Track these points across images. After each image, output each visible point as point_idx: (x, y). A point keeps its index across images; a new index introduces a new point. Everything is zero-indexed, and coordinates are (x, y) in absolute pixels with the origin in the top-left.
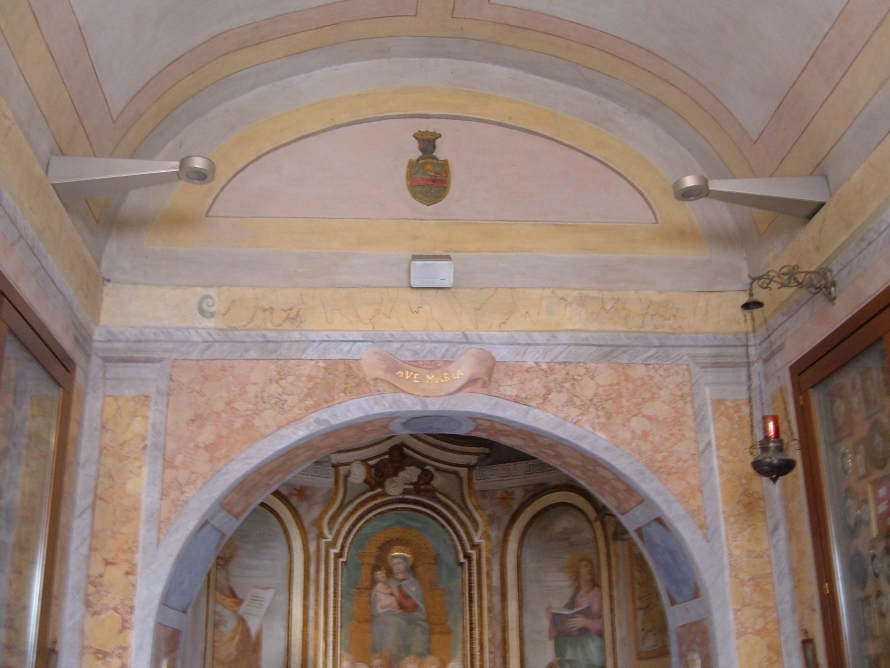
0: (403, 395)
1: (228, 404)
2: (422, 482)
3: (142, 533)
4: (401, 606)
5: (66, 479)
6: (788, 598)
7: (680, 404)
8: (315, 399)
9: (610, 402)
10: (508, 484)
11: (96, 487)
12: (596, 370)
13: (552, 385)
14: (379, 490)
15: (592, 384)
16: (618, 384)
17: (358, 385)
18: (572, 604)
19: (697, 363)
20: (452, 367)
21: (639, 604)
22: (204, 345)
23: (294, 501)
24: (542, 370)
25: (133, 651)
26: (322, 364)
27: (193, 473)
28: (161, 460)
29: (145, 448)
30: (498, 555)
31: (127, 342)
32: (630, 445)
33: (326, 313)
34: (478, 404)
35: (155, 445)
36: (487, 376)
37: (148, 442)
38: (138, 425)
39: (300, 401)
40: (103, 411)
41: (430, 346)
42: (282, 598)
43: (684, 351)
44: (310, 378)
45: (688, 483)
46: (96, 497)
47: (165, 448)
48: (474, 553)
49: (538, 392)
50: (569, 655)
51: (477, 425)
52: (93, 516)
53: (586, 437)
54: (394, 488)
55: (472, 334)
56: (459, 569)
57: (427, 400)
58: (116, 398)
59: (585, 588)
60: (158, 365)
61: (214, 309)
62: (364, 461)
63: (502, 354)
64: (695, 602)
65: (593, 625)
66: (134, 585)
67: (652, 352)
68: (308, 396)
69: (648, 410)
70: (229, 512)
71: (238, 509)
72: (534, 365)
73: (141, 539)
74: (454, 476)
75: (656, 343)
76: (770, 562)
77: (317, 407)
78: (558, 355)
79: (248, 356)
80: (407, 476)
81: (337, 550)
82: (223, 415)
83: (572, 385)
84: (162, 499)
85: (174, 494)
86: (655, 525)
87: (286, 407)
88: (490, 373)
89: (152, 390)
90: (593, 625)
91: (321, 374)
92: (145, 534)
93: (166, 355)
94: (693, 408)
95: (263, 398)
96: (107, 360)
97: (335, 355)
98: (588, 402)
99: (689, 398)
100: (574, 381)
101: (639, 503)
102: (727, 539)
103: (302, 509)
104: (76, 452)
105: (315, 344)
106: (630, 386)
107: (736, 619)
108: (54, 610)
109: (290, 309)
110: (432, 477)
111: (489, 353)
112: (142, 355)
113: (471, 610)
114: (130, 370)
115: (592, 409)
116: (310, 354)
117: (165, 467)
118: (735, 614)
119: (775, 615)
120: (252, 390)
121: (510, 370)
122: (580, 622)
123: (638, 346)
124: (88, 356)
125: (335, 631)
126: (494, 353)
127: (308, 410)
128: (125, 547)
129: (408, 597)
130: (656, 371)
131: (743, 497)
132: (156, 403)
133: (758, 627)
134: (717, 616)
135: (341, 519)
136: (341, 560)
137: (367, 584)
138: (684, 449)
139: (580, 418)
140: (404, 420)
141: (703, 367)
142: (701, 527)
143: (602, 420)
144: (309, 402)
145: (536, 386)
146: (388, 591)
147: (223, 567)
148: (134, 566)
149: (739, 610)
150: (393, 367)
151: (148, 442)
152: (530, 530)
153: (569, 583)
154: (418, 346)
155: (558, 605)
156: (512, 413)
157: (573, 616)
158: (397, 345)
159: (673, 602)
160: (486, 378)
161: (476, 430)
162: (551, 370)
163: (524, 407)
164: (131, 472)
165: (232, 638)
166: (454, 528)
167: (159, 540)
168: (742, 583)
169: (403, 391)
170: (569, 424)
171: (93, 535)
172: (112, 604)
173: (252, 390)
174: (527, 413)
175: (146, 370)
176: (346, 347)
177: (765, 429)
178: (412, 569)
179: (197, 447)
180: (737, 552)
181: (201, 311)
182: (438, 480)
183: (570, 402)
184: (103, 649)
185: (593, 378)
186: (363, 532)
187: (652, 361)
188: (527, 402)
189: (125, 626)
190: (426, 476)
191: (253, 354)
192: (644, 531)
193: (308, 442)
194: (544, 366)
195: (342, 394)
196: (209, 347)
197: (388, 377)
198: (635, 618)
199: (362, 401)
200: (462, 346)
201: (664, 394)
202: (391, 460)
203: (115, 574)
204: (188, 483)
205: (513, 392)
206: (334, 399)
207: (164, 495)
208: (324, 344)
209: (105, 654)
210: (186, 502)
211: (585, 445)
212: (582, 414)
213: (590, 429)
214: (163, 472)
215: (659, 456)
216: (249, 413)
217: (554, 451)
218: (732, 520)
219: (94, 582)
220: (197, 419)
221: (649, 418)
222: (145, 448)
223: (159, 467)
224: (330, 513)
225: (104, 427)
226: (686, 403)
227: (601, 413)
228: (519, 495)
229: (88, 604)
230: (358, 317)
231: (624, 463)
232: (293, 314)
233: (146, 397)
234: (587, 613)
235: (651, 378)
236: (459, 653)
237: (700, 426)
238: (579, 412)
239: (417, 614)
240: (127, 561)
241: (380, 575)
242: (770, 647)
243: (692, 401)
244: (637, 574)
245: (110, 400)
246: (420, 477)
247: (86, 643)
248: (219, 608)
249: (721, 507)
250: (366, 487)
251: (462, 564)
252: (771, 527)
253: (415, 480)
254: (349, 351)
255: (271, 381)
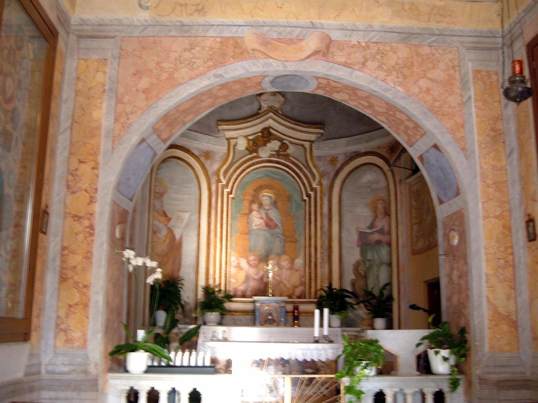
0: (271, 60)
1: (158, 64)
2: (281, 150)
3: (102, 143)
4: (267, 225)
5: (53, 105)
6: (517, 196)
7: (452, 72)
8: (214, 61)
9: (406, 69)
10: (334, 152)
11: (73, 116)
12: (397, 48)
13: (368, 56)
14: (255, 154)
15: (395, 57)
16: (412, 57)
17: (242, 53)
18: (372, 226)
19: (464, 47)
20: (303, 43)
21: (414, 221)
22: (142, 28)
23: (202, 159)
24: (362, 46)
25: (97, 216)
26: (218, 40)
27: (135, 106)
28: (114, 99)
29: (104, 91)
30: (327, 195)
31: (93, 25)
32: (418, 96)
33: (221, 7)
34: (320, 68)
35: (111, 90)
36: (326, 49)
37: (107, 88)
38: (100, 77)
39: (204, 62)
40: (77, 69)
41: (289, 29)
42: (195, 217)
43: (455, 38)
44: (211, 48)
45: (455, 121)
46: (74, 121)
47: (117, 91)
48: (312, 193)
49: (359, 60)
50: (369, 256)
51: (319, 83)
52: (71, 133)
53: (390, 90)
54: (265, 153)
55: (316, 21)
56: (303, 203)
57: (286, 63)
58: (86, 60)
59: (380, 216)
60: (112, 40)
61: (148, 4)
62: (246, 137)
63: (336, 36)
64: (456, 199)
65: (384, 238)
66: (97, 176)
67: (434, 38)
68: (208, 60)
69: (430, 75)
70: (159, 136)
71: (164, 136)
72: (356, 43)
73: (102, 148)
74: (301, 147)
75: (437, 32)
76: (506, 174)
77: (215, 66)
78: (372, 38)
79: (170, 34)
80: (272, 146)
81: (229, 190)
82: (154, 71)
83: (382, 57)
84: (115, 123)
85: (123, 120)
86: (433, 150)
87: (195, 66)
88: (328, 47)
89: (109, 55)
90: (384, 238)
91: (218, 46)
92: (104, 144)
93: (118, 34)
94: (460, 75)
95: (180, 61)
96: (80, 37)
97: (227, 34)
98: (391, 68)
99: (458, 69)
100: (383, 55)
101: (422, 136)
102: (479, 158)
103: (207, 164)
104: (60, 91)
105: (214, 27)
106: (419, 59)
107: (483, 208)
108: (46, 188)
109: (198, 5)
110: (287, 148)
111: (328, 35)
112: (102, 34)
113: (310, 228)
114: (95, 43)
115: (394, 73)
116: (211, 33)
117: (117, 103)
118: (483, 205)
119: (508, 207)
120: (173, 55)
121: (341, 46)
122: (377, 237)
123: (425, 34)
124: (68, 33)
125: (227, 238)
126: (331, 35)
127: (209, 68)
128: (92, 152)
129: (271, 220)
130: (436, 50)
131: (491, 132)
132: (112, 64)
133: (497, 214)
134: (471, 205)
135: (231, 171)
136: (231, 196)
137: (247, 212)
138: (454, 100)
139: (386, 78)
140: (271, 79)
141: (467, 49)
142: (463, 149)
143: (401, 79)
144: (210, 63)
145: (358, 57)
146: (259, 216)
147: (158, 198)
148: (98, 164)
149: (485, 202)
150: (266, 42)
151: (107, 88)
152: (347, 180)
153: (370, 214)
154: (281, 29)
155: (364, 227)
156: (341, 74)
157: (372, 233)
158: (268, 28)
159: (441, 202)
160: (325, 51)
161: (318, 88)
162: (368, 47)
163: (350, 69)
164: (95, 106)
165: (165, 241)
166: (300, 178)
167: (113, 148)
168: (488, 186)
169: (271, 58)
170: (379, 82)
171: (72, 144)
172: (84, 187)
173: (173, 55)
174: (352, 73)
175: (106, 43)
176: (235, 29)
177: (514, 68)
178: (274, 204)
179: (138, 90)
180: (485, 166)
181: (141, 6)
182: (291, 150)
183: (380, 67)
184: (77, 214)
185: (395, 53)
186: (245, 180)
187: (434, 44)
188: (351, 66)
189: (92, 201)
190: (284, 147)
191: (174, 33)
192: (424, 157)
193: (209, 90)
194: (364, 44)
195: (232, 59)
196: (145, 29)
197: (262, 49)
198: (412, 230)
199: (245, 63)
200: (310, 29)
201: (442, 65)
202: (263, 136)
203: (86, 168)
204: (132, 113)
205: (343, 60)
206: (226, 62)
207: (116, 120)
208: (220, 27)
209: (80, 218)
210: (130, 125)
211: (389, 95)
212: (388, 75)
213: (392, 85)
214: (116, 106)
215: (437, 104)
216: (171, 70)
217: (368, 102)
218: (483, 146)
219: (73, 173)
220: (138, 74)
221: (431, 80)
222: (104, 91)
223: (113, 103)
224: (225, 167)
225: (78, 78)
226: (455, 71)
227: (400, 75)
228: (341, 159)
229: (68, 187)
230: (242, 10)
231: (415, 110)
232: (200, 7)
233: (105, 59)
234: (381, 231)
235: (433, 55)
236: (302, 254)
237: (464, 86)
238: (386, 74)
239: (277, 230)
240: (92, 160)
241: (255, 206)
242: (504, 226)
243: (460, 71)
244: (414, 203)
245: (82, 62)
246: (280, 147)
247: (67, 210)
248: (156, 223)
249: (476, 137)
250: (247, 152)
251: (305, 201)
252: (508, 152)
253: (277, 149)
254: (236, 32)
255: (185, 50)
